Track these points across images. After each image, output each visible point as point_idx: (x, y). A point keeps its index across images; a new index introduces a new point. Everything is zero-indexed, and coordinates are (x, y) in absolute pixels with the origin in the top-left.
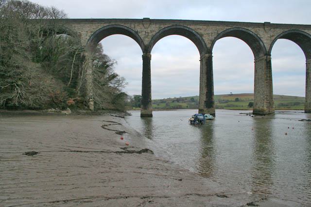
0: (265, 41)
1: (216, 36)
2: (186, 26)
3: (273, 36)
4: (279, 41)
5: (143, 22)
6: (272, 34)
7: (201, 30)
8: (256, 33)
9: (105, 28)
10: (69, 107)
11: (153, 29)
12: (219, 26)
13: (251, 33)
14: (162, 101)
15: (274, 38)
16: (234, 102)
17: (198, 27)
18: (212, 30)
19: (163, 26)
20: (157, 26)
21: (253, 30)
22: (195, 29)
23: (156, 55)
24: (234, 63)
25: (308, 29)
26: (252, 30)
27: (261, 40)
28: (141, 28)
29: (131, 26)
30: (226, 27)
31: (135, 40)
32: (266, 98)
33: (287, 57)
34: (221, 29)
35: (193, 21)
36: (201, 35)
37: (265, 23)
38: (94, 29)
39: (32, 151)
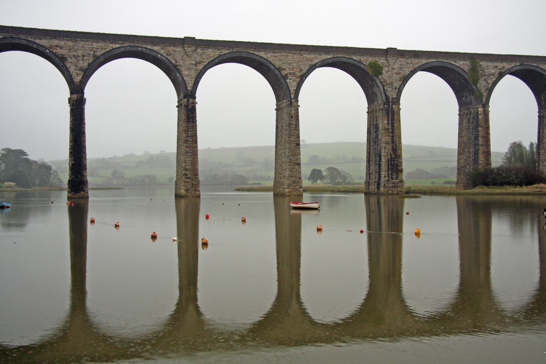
0: (185, 72)
1: (90, 61)
2: (33, 40)
3: (200, 63)
4: (420, 75)
7: (177, 56)
10: (484, 110)
12: (98, 42)
13: (159, 56)
15: (200, 67)
16: (132, 182)
17: (56, 42)
18: (489, 68)
21: (162, 52)
22: (51, 47)
23: (90, 90)
24: (237, 104)
25: (265, 51)
27: (178, 70)
30: (111, 45)
32: (186, 175)
34: (212, 53)
36: (181, 61)
37: (388, 48)
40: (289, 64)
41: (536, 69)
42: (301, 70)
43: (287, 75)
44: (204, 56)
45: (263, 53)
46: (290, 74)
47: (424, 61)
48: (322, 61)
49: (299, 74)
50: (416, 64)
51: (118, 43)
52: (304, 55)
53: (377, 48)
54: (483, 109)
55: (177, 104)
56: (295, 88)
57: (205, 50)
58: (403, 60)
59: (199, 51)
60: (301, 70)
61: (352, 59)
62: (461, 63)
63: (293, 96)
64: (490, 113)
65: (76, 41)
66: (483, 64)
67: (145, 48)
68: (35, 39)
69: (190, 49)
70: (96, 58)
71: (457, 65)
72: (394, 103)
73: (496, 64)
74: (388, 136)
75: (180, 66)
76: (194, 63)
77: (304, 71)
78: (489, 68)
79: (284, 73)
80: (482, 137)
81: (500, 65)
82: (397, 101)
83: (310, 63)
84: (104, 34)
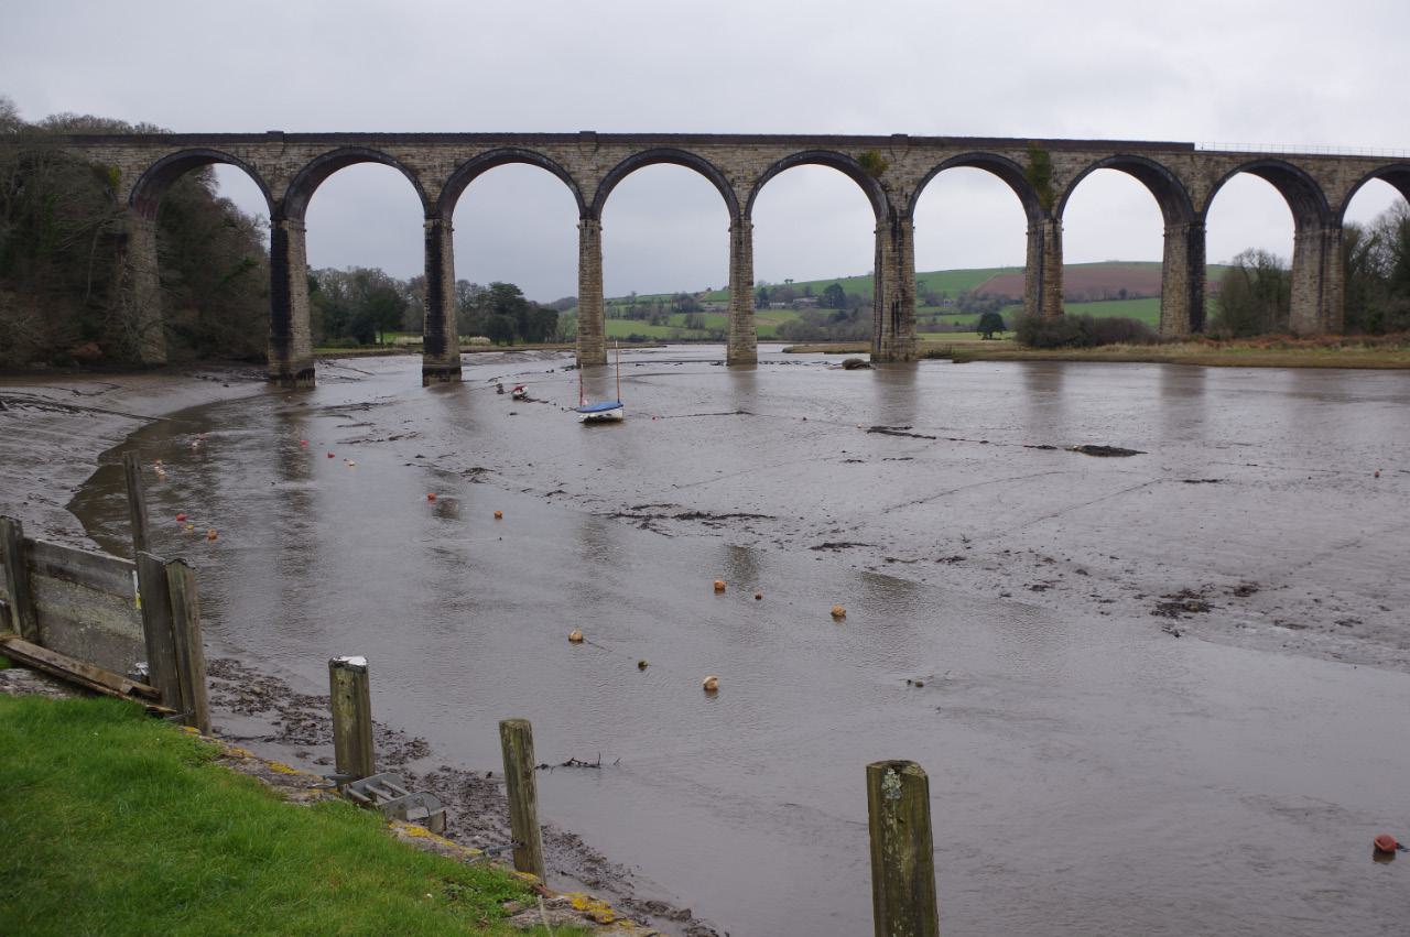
3: (603, 167)
5: (578, 141)
6: (601, 162)
8: (559, 162)
9: (175, 158)
10: (1054, 227)
11: (295, 159)
12: (461, 146)
14: (630, 300)
17: (406, 150)
19: (316, 151)
20: (304, 150)
21: (549, 154)
22: (399, 157)
26: (1162, 159)
28: (263, 158)
29: (237, 152)
31: (712, 181)
33: (1372, 206)
34: (781, 154)
35: (454, 134)
37: (582, 133)
38: (145, 160)
39: (1137, 347)
40: (737, 164)
41: (1145, 163)
42: (755, 173)
43: (733, 180)
44: (609, 158)
45: (697, 149)
46: (739, 178)
47: (953, 154)
48: (788, 158)
49: (751, 178)
50: (941, 157)
51: (487, 146)
52: (761, 150)
53: (458, 132)
54: (1052, 225)
55: (753, 230)
56: (746, 200)
57: (611, 150)
58: (918, 154)
59: (602, 150)
60: (755, 173)
61: (836, 153)
62: (1016, 154)
63: (742, 212)
64: (1064, 233)
65: (432, 146)
66: (1054, 155)
67: (526, 150)
68: (379, 146)
69: (587, 149)
70: (458, 167)
71: (1009, 157)
72: (902, 218)
73: (1074, 155)
74: (894, 268)
75: (574, 173)
76: (594, 168)
77: (761, 174)
78: (1061, 162)
79: (729, 177)
80: (1050, 270)
81: (1081, 157)
82: (908, 215)
83: (769, 161)
84: (432, 135)
